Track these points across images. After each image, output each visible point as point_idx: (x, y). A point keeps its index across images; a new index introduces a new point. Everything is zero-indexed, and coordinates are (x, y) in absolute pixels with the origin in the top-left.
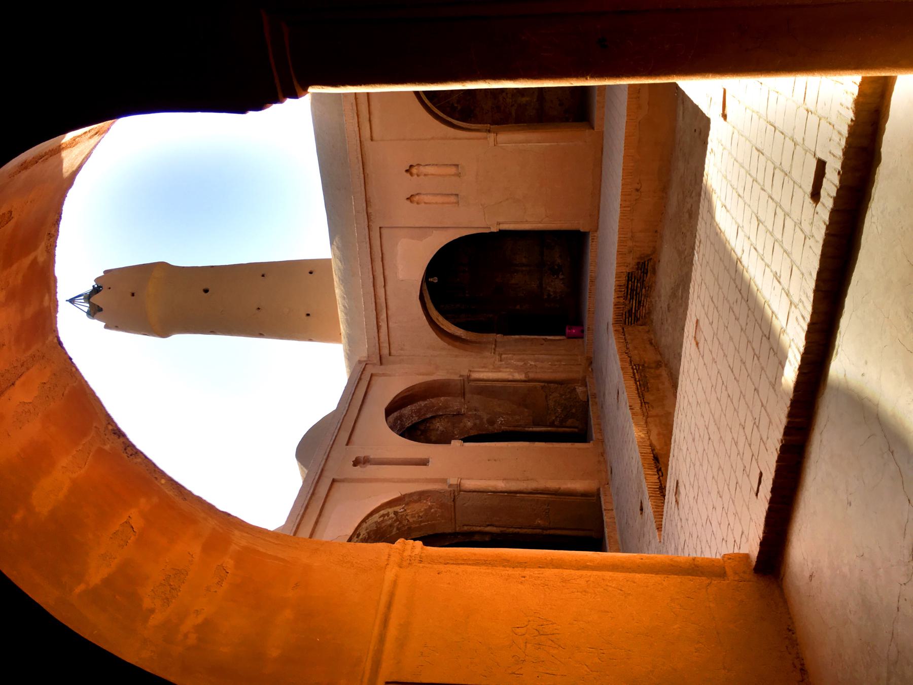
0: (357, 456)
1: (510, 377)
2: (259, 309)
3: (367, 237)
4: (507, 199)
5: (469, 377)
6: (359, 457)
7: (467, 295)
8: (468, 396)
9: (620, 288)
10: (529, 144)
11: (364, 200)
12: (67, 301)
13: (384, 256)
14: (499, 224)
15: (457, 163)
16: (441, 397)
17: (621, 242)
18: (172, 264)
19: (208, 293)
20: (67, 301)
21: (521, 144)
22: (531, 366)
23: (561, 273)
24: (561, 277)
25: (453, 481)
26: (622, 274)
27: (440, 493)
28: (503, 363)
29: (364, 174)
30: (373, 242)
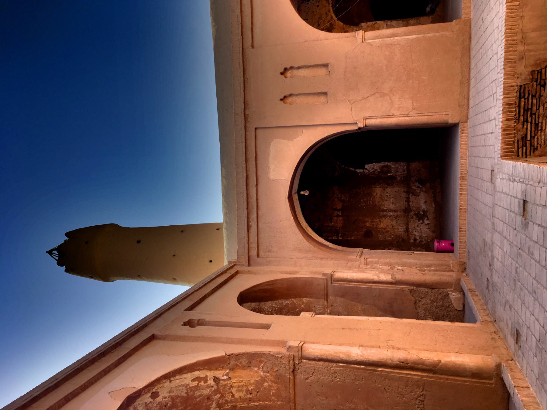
0: (191, 318)
1: (376, 278)
2: (174, 256)
3: (244, 137)
4: (374, 94)
5: (332, 275)
6: (193, 320)
7: (340, 238)
8: (331, 297)
9: (509, 108)
10: (396, 38)
11: (243, 101)
12: (47, 252)
13: (258, 156)
14: (366, 119)
15: (325, 62)
16: (303, 297)
17: (509, 46)
18: (120, 226)
19: (140, 243)
20: (47, 252)
21: (388, 39)
22: (398, 271)
23: (426, 218)
24: (426, 222)
25: (294, 343)
26: (512, 88)
27: (277, 358)
28: (368, 266)
29: (244, 77)
30: (248, 142)
